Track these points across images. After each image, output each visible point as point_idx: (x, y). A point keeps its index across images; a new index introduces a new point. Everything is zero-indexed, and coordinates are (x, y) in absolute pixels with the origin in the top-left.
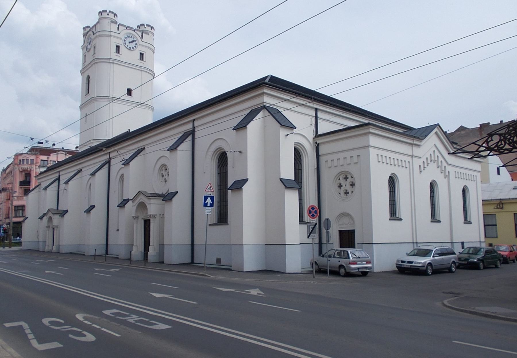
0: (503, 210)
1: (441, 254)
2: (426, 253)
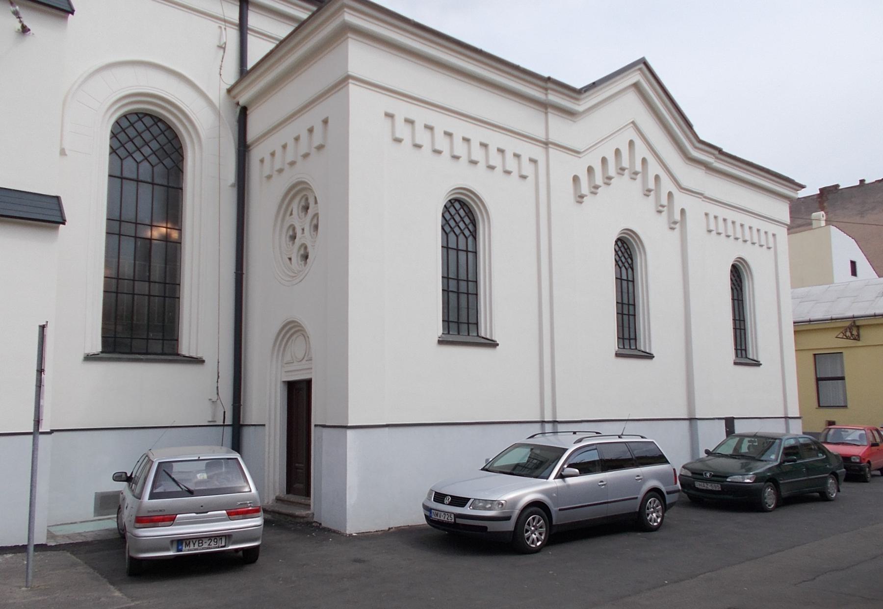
0: (859, 343)
1: (585, 468)
2: (537, 464)
